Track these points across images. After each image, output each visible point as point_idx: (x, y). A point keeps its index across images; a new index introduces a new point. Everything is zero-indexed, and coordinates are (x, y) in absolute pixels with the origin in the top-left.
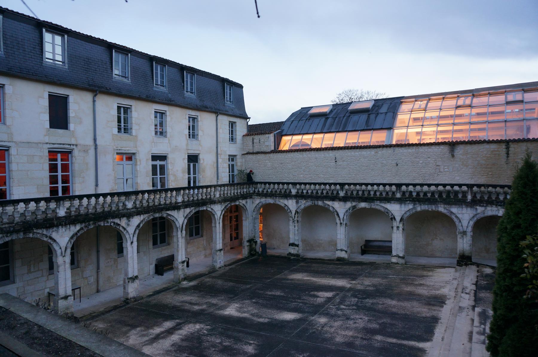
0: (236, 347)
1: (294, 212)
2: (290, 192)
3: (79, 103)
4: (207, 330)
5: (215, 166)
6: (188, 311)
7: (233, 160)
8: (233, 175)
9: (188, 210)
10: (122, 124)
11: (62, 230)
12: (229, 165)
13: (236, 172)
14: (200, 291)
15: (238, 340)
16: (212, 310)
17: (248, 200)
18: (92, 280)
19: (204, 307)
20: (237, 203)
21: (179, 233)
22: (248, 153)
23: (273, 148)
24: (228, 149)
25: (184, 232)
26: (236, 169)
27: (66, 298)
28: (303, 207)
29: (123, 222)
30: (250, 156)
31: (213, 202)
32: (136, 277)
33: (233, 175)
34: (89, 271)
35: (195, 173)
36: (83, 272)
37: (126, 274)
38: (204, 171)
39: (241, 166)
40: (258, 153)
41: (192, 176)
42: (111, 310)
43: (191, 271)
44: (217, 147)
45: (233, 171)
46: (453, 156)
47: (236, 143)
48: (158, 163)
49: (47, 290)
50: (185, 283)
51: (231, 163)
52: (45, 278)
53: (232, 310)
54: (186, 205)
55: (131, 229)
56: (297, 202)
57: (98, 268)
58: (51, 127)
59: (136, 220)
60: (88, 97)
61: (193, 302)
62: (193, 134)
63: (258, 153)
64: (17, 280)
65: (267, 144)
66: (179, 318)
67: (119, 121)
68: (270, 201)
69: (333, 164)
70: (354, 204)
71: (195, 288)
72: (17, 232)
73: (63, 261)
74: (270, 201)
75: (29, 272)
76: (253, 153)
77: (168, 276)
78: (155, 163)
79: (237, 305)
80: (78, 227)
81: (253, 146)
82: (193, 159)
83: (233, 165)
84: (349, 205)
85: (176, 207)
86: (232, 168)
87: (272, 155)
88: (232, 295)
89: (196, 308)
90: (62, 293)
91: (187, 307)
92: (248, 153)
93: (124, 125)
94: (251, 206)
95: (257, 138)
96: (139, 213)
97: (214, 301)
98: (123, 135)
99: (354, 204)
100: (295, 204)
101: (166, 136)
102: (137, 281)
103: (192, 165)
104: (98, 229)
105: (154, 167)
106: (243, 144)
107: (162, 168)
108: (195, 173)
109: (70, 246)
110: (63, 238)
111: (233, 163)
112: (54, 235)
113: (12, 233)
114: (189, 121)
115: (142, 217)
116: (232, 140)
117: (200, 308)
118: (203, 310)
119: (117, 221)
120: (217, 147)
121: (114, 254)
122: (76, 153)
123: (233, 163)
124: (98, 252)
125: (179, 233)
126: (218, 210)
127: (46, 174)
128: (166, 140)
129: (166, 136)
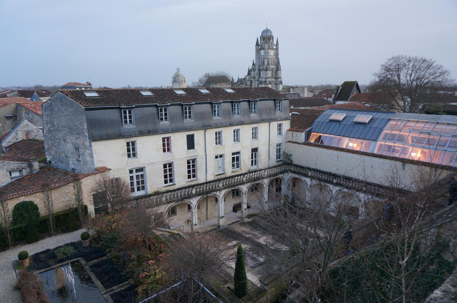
0: (257, 258)
1: (309, 186)
2: (308, 174)
3: (198, 136)
4: (249, 248)
5: (268, 152)
6: (243, 237)
7: (280, 145)
8: (280, 155)
9: (249, 184)
10: (218, 140)
11: (194, 199)
12: (277, 149)
13: (281, 153)
14: (252, 226)
15: (259, 255)
16: (253, 238)
17: (285, 174)
18: (205, 214)
19: (251, 236)
20: (278, 177)
21: (244, 195)
22: (289, 142)
23: (304, 141)
24: (276, 139)
25: (246, 195)
26: (282, 151)
27: (196, 225)
28: (314, 183)
29: (218, 193)
30: (290, 144)
31: (263, 178)
32: (223, 217)
33: (280, 155)
34: (204, 210)
35: (255, 157)
36: (201, 210)
37: (219, 215)
38: (261, 156)
39: (285, 149)
40: (295, 143)
41: (254, 159)
42: (212, 231)
43: (251, 211)
44: (269, 141)
45: (280, 152)
46: (404, 169)
47: (282, 135)
48: (235, 156)
49: (188, 218)
50: (246, 219)
51: (278, 147)
52: (186, 213)
53: (262, 240)
54: (248, 181)
55: (221, 196)
56: (311, 180)
57: (207, 209)
58: (188, 149)
59: (223, 192)
60: (202, 132)
61: (247, 232)
62: (255, 136)
63: (295, 143)
64: (177, 214)
65: (300, 138)
66: (239, 240)
67: (216, 139)
68: (297, 176)
69: (336, 158)
70: (341, 188)
71: (250, 223)
72: (179, 201)
73: (195, 210)
74: (297, 176)
75: (181, 211)
76: (292, 142)
77: (239, 214)
78: (234, 156)
79: (265, 238)
80: (200, 197)
81: (292, 138)
82: (255, 150)
83: (280, 149)
84: (338, 188)
85: (243, 183)
86: (278, 151)
87: (302, 146)
88: (265, 231)
89: (248, 236)
90: (194, 223)
91: (244, 234)
92: (289, 142)
93: (218, 139)
94: (287, 177)
95: (295, 133)
96: (224, 189)
97: (256, 233)
98: (219, 146)
99: (341, 188)
100: (310, 181)
101: (239, 142)
102: (224, 218)
103: (254, 153)
104: (207, 192)
105: (233, 159)
106: (287, 135)
107: (238, 158)
108: (255, 157)
109: (197, 205)
110: (194, 202)
111: (280, 147)
112: (191, 201)
113: (178, 201)
114: (253, 130)
115: (226, 190)
116: (280, 133)
117: (249, 236)
118: (250, 238)
119: (215, 193)
120: (269, 141)
121: (214, 203)
122: (198, 159)
123: (280, 147)
124: (207, 202)
125: (244, 195)
126: (266, 182)
127: (186, 170)
128: (239, 144)
129: (239, 142)
